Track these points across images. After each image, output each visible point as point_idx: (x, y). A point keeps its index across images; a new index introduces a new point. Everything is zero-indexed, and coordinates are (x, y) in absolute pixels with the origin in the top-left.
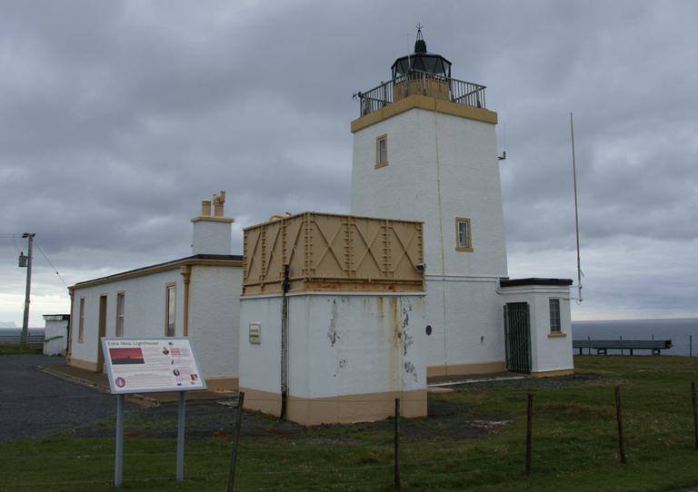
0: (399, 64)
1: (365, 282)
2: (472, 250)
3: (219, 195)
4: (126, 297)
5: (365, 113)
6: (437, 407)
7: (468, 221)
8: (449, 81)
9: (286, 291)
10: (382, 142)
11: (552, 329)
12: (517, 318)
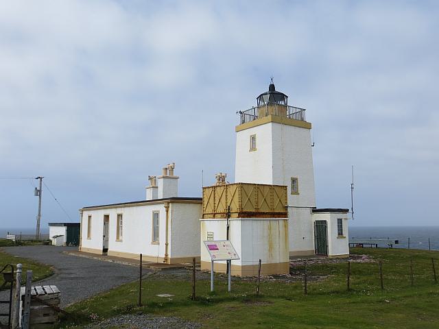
2: (298, 194)
3: (171, 165)
5: (244, 122)
6: (293, 270)
7: (297, 179)
8: (286, 106)
10: (253, 138)
11: (339, 234)
12: (321, 228)
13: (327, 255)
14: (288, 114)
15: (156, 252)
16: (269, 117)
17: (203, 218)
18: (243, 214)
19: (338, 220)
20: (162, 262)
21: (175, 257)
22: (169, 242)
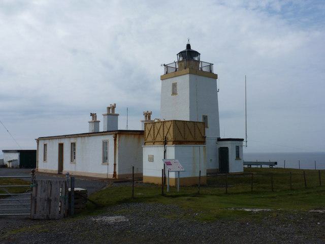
0: (181, 54)
1: (189, 142)
4: (48, 146)
8: (199, 61)
9: (165, 145)
10: (174, 85)
11: (237, 157)
13: (228, 172)
14: (200, 66)
15: (106, 171)
16: (188, 70)
17: (145, 145)
18: (177, 142)
19: (236, 146)
20: (111, 177)
21: (121, 173)
22: (117, 163)
